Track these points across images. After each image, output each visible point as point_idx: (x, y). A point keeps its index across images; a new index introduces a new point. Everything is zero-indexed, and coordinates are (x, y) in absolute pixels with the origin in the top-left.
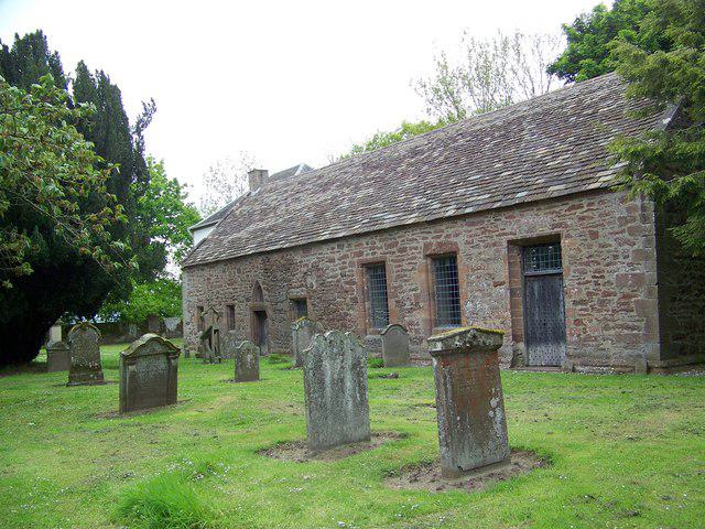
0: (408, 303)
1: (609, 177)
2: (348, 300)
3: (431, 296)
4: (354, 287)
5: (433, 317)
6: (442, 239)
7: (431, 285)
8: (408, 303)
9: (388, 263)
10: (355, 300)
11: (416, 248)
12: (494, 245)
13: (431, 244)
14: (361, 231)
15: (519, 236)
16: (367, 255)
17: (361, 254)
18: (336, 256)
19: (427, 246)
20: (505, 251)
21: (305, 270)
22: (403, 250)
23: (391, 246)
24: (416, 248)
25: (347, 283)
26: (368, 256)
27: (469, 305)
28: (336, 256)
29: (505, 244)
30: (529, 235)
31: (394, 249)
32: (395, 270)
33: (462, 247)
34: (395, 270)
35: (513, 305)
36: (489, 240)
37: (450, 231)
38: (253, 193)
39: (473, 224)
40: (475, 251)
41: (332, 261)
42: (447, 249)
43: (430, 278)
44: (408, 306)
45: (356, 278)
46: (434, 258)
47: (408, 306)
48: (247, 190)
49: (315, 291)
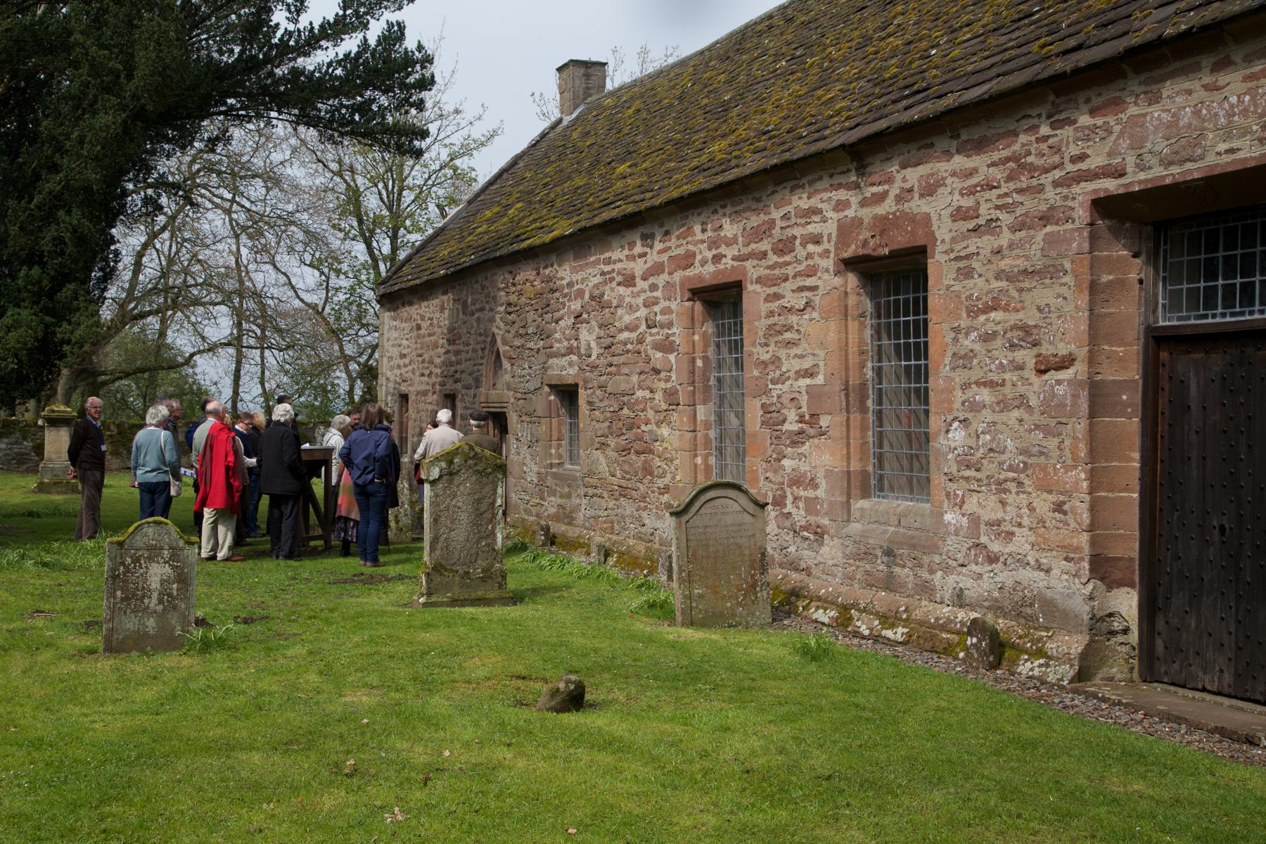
0: (792, 415)
1: (1027, 30)
2: (659, 396)
3: (854, 396)
4: (672, 357)
5: (855, 466)
6: (888, 207)
7: (854, 359)
8: (792, 415)
9: (750, 288)
10: (671, 397)
11: (817, 240)
12: (1045, 219)
13: (857, 222)
14: (687, 189)
15: (1136, 179)
16: (704, 263)
17: (687, 260)
18: (639, 267)
19: (846, 230)
20: (1080, 242)
21: (576, 306)
22: (784, 247)
23: (758, 234)
24: (817, 240)
25: (659, 347)
26: (705, 272)
27: (958, 436)
28: (639, 267)
29: (1082, 214)
30: (1175, 173)
31: (765, 246)
32: (764, 308)
33: (943, 231)
34: (764, 308)
35: (1098, 448)
36: (1031, 205)
37: (913, 176)
38: (567, 120)
39: (979, 146)
40: (986, 243)
41: (629, 281)
42: (901, 240)
43: (853, 337)
44: (791, 426)
45: (677, 333)
46: (859, 265)
47: (791, 426)
48: (556, 115)
49: (594, 367)
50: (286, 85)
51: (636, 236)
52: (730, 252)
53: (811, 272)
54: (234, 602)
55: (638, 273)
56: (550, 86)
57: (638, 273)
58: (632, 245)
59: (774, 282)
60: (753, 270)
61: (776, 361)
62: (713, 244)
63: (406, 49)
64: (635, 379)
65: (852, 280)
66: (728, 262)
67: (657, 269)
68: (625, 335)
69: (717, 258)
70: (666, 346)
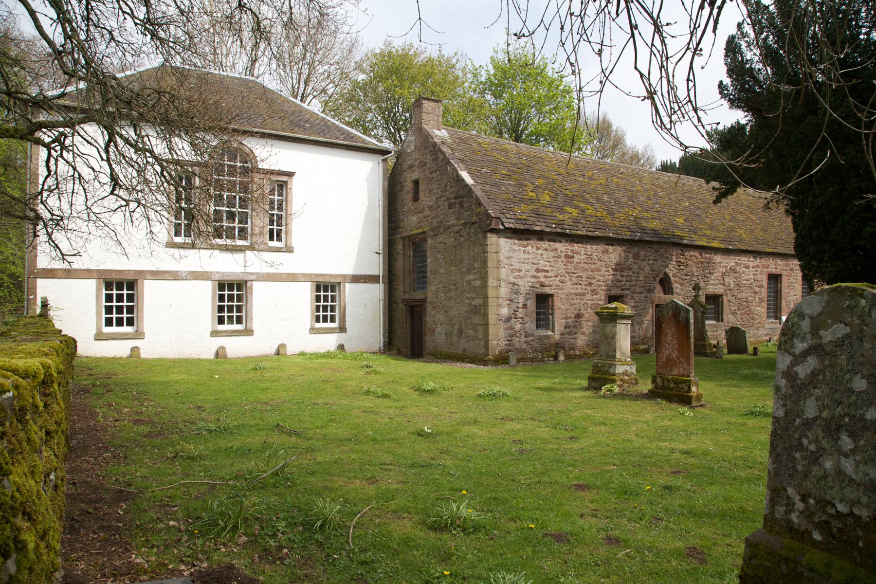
2: (757, 299)
17: (768, 267)
18: (751, 264)
23: (788, 265)
25: (757, 286)
28: (751, 264)
31: (787, 268)
41: (747, 267)
50: (784, 53)
51: (751, 256)
52: (779, 268)
53: (797, 276)
54: (445, 401)
55: (751, 266)
56: (59, 328)
57: (751, 266)
58: (749, 258)
59: (789, 276)
60: (784, 273)
61: (789, 292)
62: (775, 265)
63: (576, 164)
64: (749, 294)
65: (597, 317)
66: (778, 270)
67: (758, 266)
68: (745, 282)
69: (776, 268)
70: (761, 287)
